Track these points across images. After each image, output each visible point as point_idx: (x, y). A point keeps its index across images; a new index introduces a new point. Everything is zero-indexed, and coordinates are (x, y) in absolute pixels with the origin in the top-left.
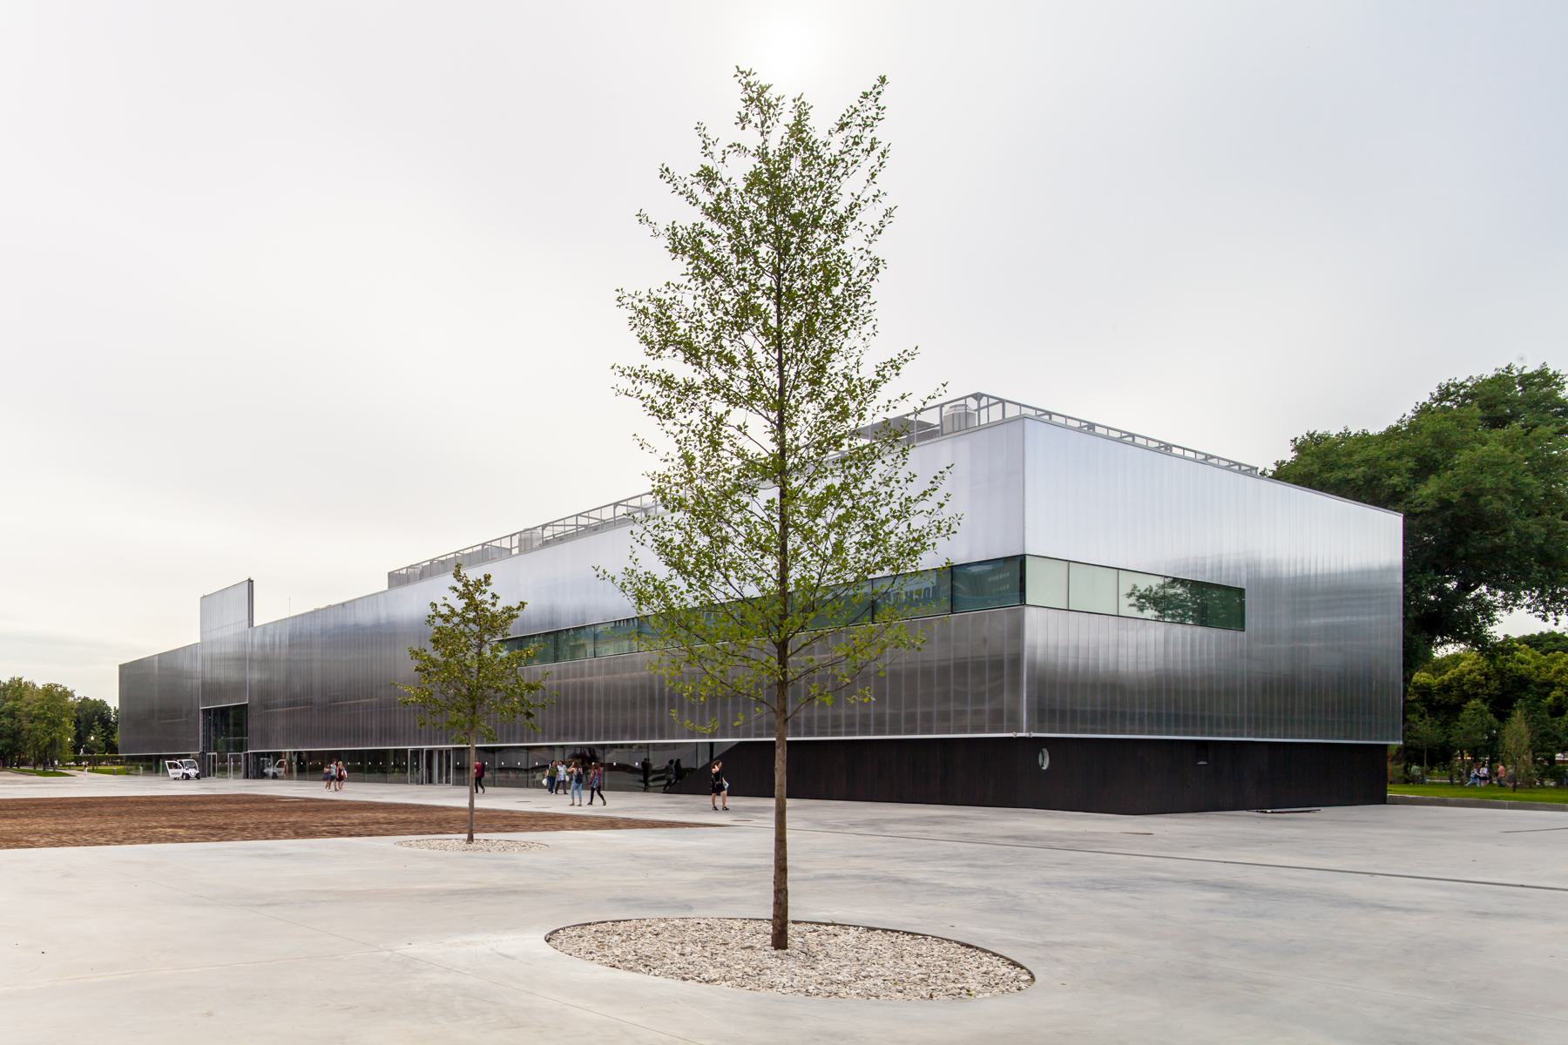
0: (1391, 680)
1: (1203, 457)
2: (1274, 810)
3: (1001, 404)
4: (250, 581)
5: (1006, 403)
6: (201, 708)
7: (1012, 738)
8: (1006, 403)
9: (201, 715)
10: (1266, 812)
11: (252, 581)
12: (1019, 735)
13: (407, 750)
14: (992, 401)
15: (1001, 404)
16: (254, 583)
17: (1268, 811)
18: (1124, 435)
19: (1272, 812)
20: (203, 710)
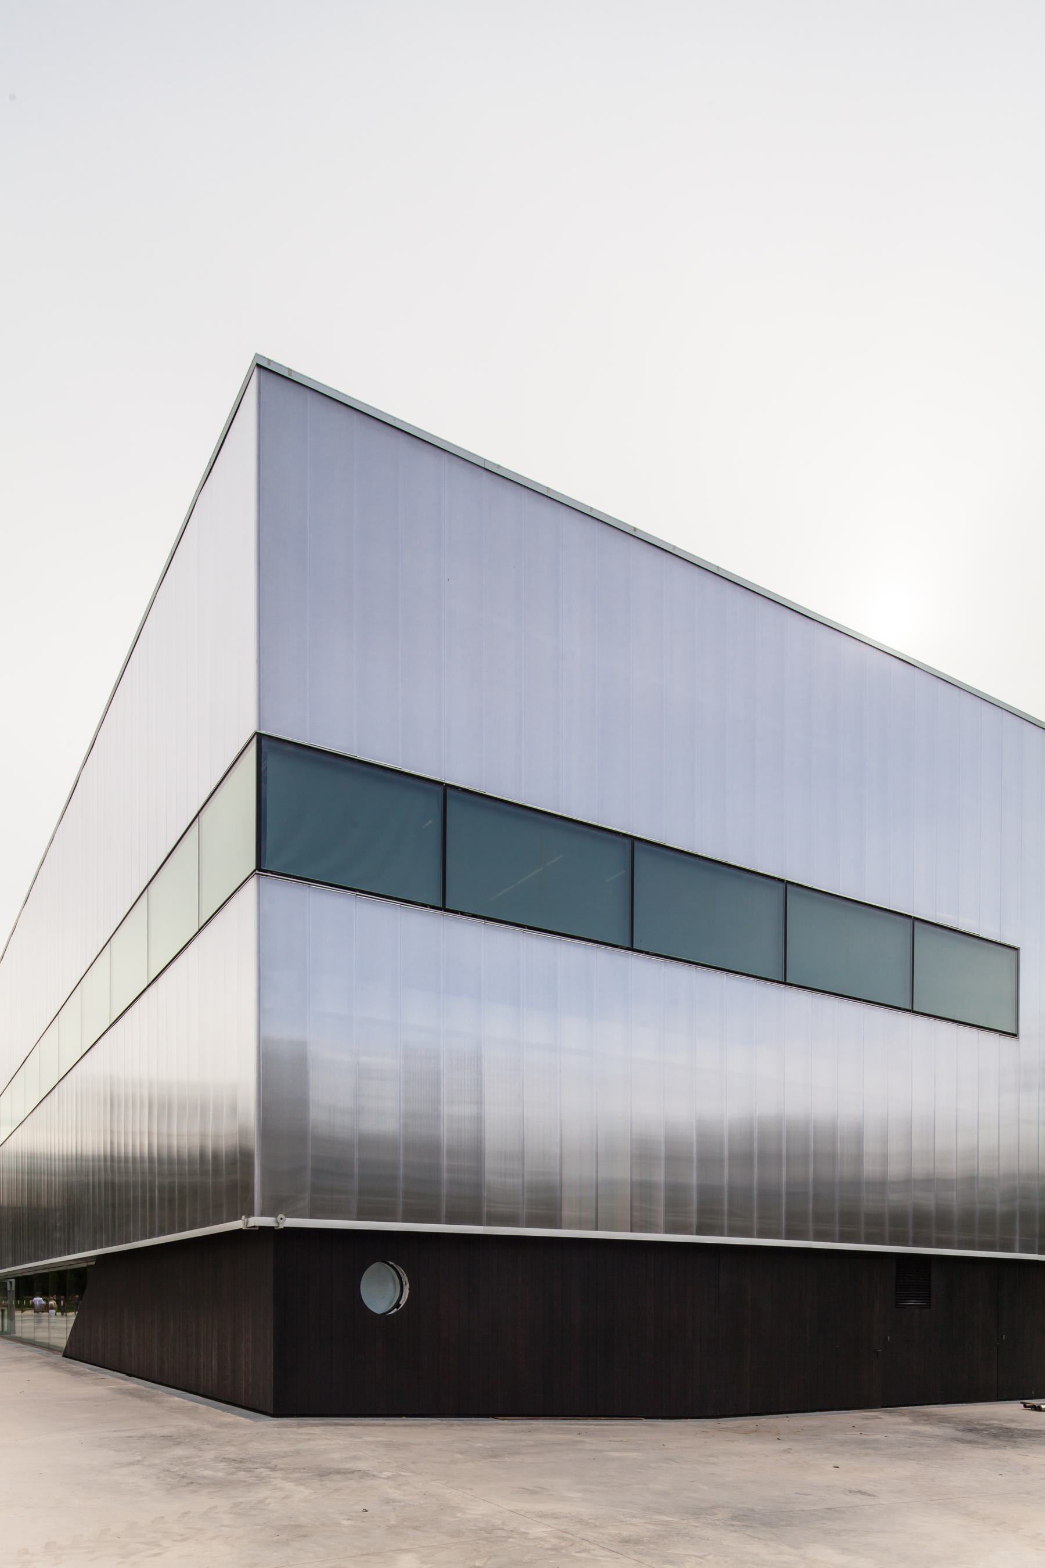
7: (239, 1231)
12: (257, 1221)
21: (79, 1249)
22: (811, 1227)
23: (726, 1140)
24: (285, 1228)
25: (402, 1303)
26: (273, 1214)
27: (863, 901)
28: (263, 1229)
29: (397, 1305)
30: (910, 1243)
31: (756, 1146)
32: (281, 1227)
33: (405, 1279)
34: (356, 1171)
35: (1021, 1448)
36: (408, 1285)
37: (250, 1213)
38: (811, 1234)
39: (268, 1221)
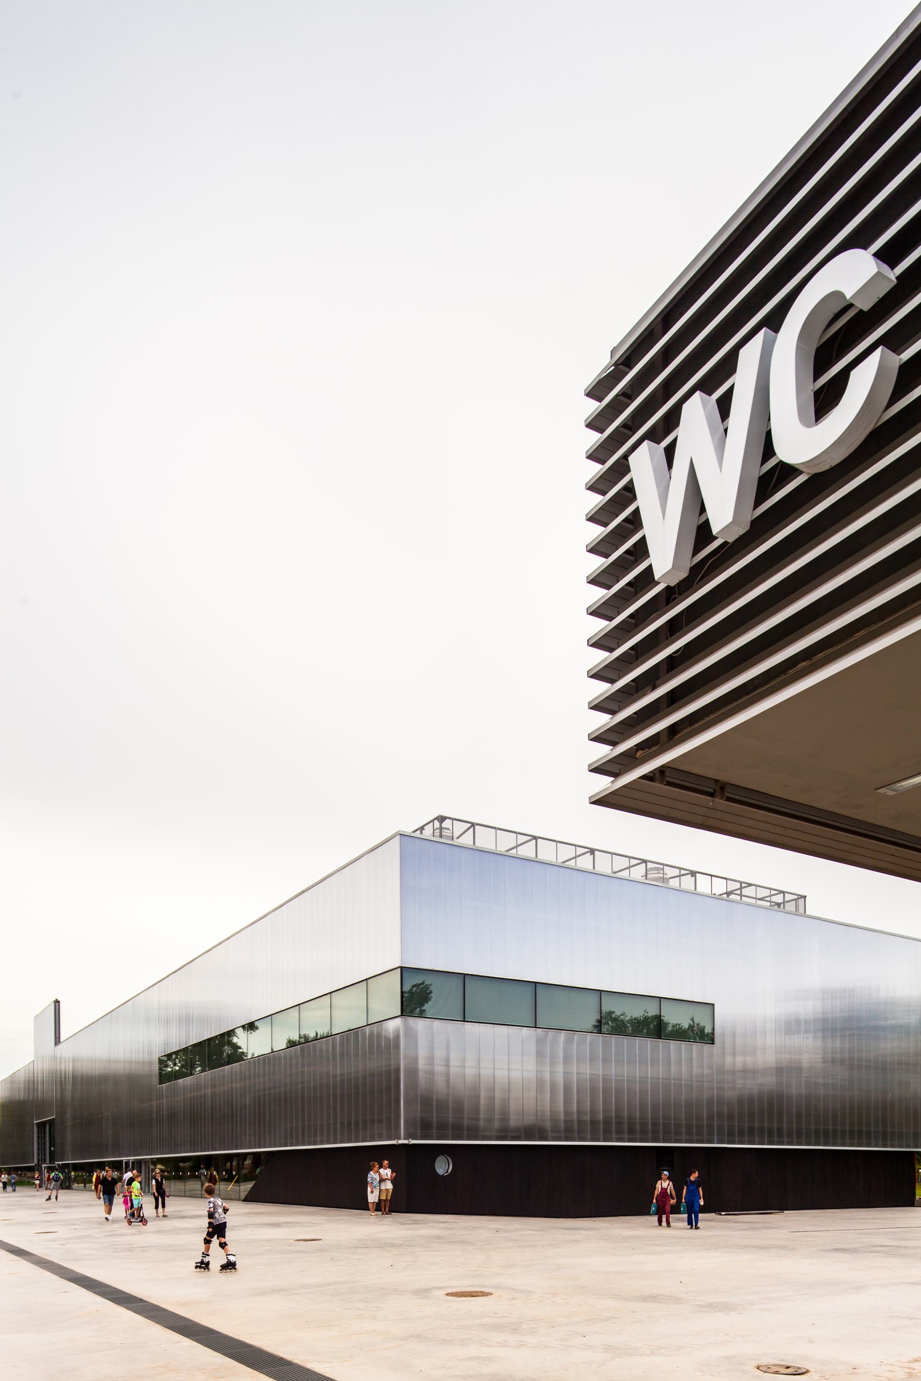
0: (202, 1082)
1: (738, 885)
2: (727, 1213)
3: (534, 840)
4: (57, 1002)
5: (786, 894)
6: (35, 1122)
7: (394, 1145)
8: (786, 894)
9: (35, 1128)
10: (721, 1215)
11: (59, 1002)
12: (401, 1142)
13: (122, 1161)
14: (683, 872)
15: (534, 840)
16: (715, 1005)
17: (722, 1213)
18: (773, 892)
19: (726, 1215)
20: (36, 1123)
21: (142, 1153)
22: (550, 1134)
23: (766, 1095)
24: (412, 1144)
25: (449, 1171)
26: (407, 1139)
27: (883, 844)
28: (402, 1145)
29: (447, 1172)
30: (776, 1144)
31: (715, 1097)
32: (410, 1143)
33: (450, 1161)
34: (626, 1121)
35: (146, 1232)
36: (452, 1164)
37: (399, 1138)
38: (785, 1142)
39: (406, 1142)
